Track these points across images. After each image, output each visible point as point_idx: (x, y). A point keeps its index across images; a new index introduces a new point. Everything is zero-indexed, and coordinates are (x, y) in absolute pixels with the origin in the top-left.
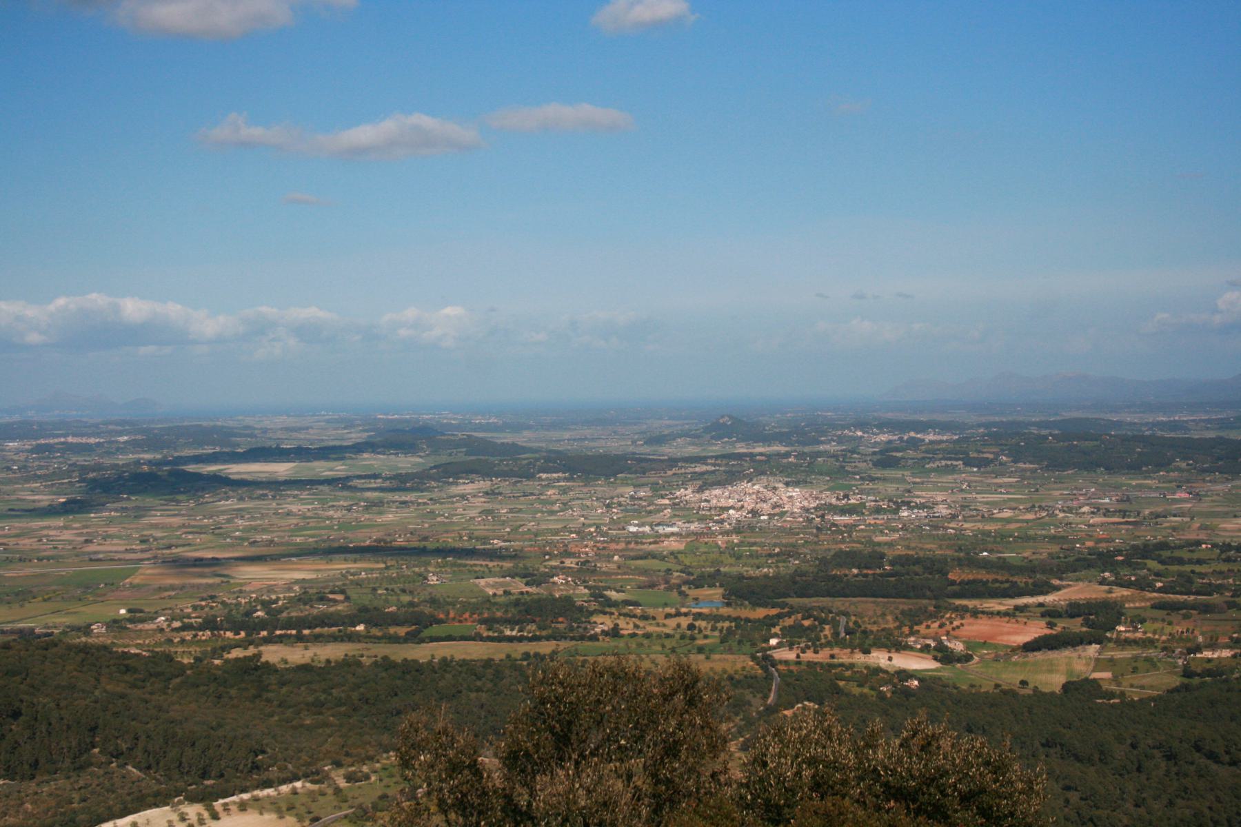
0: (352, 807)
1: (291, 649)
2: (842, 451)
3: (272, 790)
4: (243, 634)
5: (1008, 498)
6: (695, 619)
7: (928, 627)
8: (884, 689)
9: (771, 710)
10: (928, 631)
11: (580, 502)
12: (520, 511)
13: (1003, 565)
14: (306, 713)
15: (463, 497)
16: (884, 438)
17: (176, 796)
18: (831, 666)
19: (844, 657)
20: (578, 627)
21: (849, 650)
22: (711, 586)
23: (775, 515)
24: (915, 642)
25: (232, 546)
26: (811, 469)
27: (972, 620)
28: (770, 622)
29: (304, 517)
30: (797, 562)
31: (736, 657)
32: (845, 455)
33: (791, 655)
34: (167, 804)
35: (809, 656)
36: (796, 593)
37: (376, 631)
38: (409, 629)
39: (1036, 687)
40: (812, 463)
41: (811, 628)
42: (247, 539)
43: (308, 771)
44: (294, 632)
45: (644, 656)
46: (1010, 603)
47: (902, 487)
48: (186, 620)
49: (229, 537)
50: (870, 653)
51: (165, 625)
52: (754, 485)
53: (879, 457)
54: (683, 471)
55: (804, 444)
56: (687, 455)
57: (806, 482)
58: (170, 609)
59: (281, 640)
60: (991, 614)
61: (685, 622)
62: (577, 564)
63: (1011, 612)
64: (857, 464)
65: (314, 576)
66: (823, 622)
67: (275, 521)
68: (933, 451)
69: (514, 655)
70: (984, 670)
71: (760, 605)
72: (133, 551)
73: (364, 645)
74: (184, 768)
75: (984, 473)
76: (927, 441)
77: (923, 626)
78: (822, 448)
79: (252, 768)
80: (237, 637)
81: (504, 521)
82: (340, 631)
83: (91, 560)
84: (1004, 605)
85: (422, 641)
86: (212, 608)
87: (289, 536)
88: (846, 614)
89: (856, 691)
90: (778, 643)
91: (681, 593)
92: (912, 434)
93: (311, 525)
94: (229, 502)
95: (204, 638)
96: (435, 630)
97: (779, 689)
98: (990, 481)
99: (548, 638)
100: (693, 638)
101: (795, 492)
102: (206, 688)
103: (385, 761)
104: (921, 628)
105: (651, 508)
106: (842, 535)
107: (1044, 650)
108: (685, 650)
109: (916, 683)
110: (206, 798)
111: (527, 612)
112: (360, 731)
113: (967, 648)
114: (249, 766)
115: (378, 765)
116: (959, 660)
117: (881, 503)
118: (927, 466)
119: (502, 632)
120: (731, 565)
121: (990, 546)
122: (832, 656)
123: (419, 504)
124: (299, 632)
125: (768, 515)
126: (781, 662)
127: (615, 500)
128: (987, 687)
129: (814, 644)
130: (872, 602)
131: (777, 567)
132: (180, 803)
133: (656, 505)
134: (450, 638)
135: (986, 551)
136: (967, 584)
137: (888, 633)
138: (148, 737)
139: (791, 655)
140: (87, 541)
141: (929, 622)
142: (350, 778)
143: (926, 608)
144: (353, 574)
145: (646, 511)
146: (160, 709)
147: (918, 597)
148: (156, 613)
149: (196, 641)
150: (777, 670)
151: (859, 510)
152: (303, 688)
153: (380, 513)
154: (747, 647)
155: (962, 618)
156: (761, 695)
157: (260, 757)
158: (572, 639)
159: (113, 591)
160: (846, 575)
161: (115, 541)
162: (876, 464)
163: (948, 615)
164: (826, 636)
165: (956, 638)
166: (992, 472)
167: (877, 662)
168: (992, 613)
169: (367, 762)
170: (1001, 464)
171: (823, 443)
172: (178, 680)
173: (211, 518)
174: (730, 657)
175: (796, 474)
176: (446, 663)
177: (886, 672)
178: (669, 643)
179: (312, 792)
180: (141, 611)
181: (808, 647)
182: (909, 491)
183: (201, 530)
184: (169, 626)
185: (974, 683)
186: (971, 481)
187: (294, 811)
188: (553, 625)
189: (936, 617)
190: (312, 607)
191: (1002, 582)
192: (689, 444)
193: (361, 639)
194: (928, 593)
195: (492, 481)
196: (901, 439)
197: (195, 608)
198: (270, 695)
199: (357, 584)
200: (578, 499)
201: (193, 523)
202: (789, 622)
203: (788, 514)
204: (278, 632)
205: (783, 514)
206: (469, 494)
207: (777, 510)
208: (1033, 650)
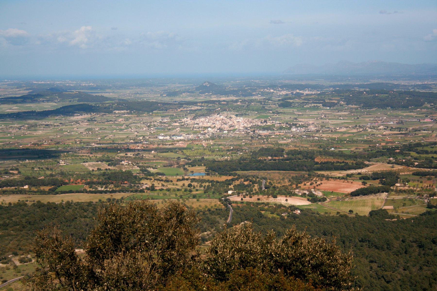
0: (23, 275)
2: (263, 99)
5: (344, 122)
6: (191, 182)
7: (305, 185)
9: (229, 226)
10: (305, 187)
11: (135, 124)
13: (341, 155)
15: (77, 122)
16: (284, 93)
18: (258, 204)
19: (264, 199)
20: (134, 186)
21: (267, 196)
23: (230, 130)
26: (248, 108)
27: (326, 181)
28: (228, 183)
30: (241, 153)
31: (212, 200)
35: (247, 199)
36: (241, 169)
37: (34, 189)
39: (357, 213)
41: (248, 186)
47: (293, 117)
50: (277, 198)
52: (220, 116)
53: (281, 102)
54: (186, 109)
55: (245, 96)
60: (335, 178)
61: (187, 183)
63: (345, 177)
66: (254, 182)
68: (308, 99)
71: (224, 175)
75: (332, 110)
76: (305, 94)
81: (97, 134)
84: (342, 174)
85: (57, 193)
88: (265, 179)
89: (270, 216)
90: (232, 193)
91: (185, 169)
92: (298, 91)
98: (335, 114)
99: (119, 191)
100: (191, 191)
101: (241, 119)
104: (302, 185)
105: (170, 127)
106: (263, 140)
107: (361, 195)
109: (299, 212)
113: (324, 195)
117: (282, 125)
118: (305, 107)
119: (97, 189)
120: (209, 155)
121: (335, 145)
123: (55, 126)
125: (228, 130)
126: (233, 202)
127: (152, 124)
128: (333, 213)
130: (278, 173)
131: (232, 156)
133: (173, 126)
134: (71, 192)
135: (333, 147)
136: (324, 164)
137: (285, 187)
141: (306, 183)
142: (21, 261)
145: (168, 129)
147: (300, 170)
150: (232, 206)
151: (272, 128)
153: (35, 130)
154: (217, 195)
155: (322, 180)
156: (224, 218)
158: (132, 191)
160: (265, 160)
163: (314, 179)
164: (255, 190)
165: (318, 190)
167: (280, 201)
168: (336, 178)
169: (30, 253)
170: (341, 105)
171: (254, 95)
174: (209, 200)
176: (69, 204)
177: (285, 207)
178: (179, 194)
181: (247, 195)
182: (296, 119)
185: (327, 212)
186: (326, 114)
188: (122, 185)
191: (341, 163)
192: (189, 96)
193: (27, 192)
194: (305, 168)
195: (91, 114)
196: (292, 93)
199: (24, 166)
200: (134, 123)
202: (237, 183)
203: (237, 130)
207: (232, 128)
208: (356, 196)
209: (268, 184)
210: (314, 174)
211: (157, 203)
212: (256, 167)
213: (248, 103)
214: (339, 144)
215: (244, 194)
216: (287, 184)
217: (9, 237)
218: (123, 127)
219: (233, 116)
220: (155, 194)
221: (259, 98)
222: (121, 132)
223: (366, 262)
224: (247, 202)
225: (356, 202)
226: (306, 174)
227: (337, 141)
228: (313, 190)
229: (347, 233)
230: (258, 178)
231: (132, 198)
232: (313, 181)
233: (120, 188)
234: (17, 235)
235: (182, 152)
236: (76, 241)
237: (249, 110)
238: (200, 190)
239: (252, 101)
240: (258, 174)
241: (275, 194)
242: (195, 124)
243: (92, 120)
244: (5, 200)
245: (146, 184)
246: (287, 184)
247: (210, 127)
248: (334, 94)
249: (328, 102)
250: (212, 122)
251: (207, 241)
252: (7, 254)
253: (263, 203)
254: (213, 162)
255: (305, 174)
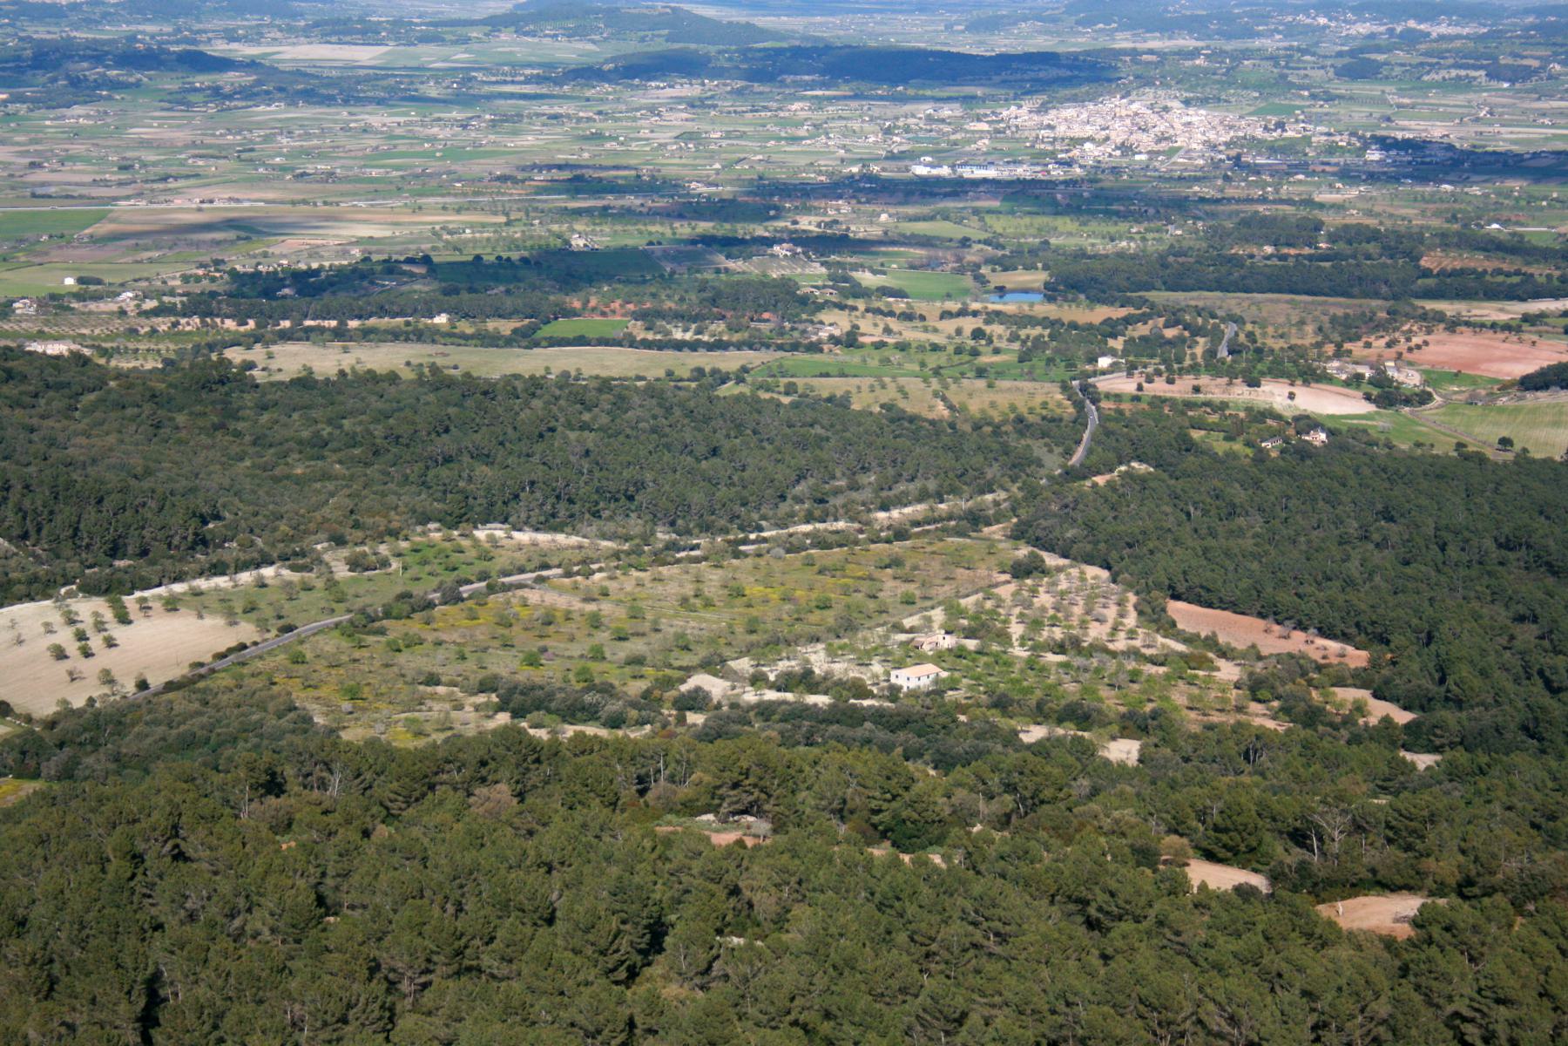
0: (349, 611)
1: (322, 350)
2: (1286, 49)
3: (226, 578)
4: (252, 324)
5: (1555, 135)
6: (987, 322)
7: (1368, 345)
8: (1267, 445)
9: (1071, 475)
10: (1367, 352)
11: (843, 123)
12: (743, 136)
13: (1516, 248)
14: (297, 456)
15: (653, 110)
16: (1363, 29)
17: (64, 585)
18: (1189, 405)
19: (1214, 389)
20: (793, 329)
21: (1226, 380)
22: (1029, 267)
23: (1158, 153)
24: (1340, 370)
25: (265, 179)
26: (1230, 79)
27: (1444, 336)
28: (1111, 329)
29: (391, 137)
30: (1179, 232)
31: (1037, 385)
32: (1291, 56)
33: (1126, 385)
34: (47, 597)
35: (1159, 387)
36: (1165, 283)
37: (466, 327)
38: (518, 325)
39: (1525, 450)
40: (1233, 68)
41: (1178, 342)
42: (293, 169)
43: (289, 551)
44: (334, 323)
45: (887, 380)
46: (1516, 309)
47: (1377, 112)
48: (166, 299)
49: (264, 164)
50: (1259, 386)
51: (130, 307)
52: (1132, 102)
53: (1347, 60)
54: (1019, 76)
55: (1229, 36)
56: (873, 44)
57: (1219, 100)
58: (147, 279)
59: (307, 335)
60: (1479, 326)
61: (969, 324)
62: (819, 225)
63: (1514, 323)
64: (1308, 72)
65: (388, 233)
66: (1196, 331)
67: (342, 140)
68: (1439, 54)
69: (678, 373)
70: (1446, 419)
71: (1103, 302)
72: (106, 184)
73: (440, 348)
74: (82, 539)
75: (1519, 91)
76: (1434, 35)
77: (1361, 344)
78: (1257, 43)
79: (195, 543)
80: (242, 329)
81: (713, 151)
82: (408, 324)
83: (34, 195)
84: (1508, 312)
85: (537, 344)
86: (213, 280)
87: (361, 167)
88: (1239, 320)
89: (1220, 446)
90: (1112, 365)
91: (979, 278)
92: (1412, 24)
93: (402, 149)
94: (273, 108)
95: (188, 328)
96: (561, 327)
97: (1093, 438)
98: (1527, 105)
99: (739, 346)
100: (975, 353)
101: (1198, 116)
102: (136, 410)
103: (418, 539)
104: (1356, 348)
105: (958, 136)
106: (1263, 189)
107: (1553, 388)
108: (955, 372)
109: (1323, 436)
110: (109, 588)
111: (714, 301)
112: (381, 488)
113: (1426, 382)
114: (190, 538)
115: (404, 545)
116: (1407, 401)
117: (1337, 138)
118: (1426, 78)
119: (669, 333)
120: (1070, 234)
121: (1506, 214)
122: (1197, 389)
123: (579, 120)
124: (342, 323)
125: (1149, 152)
126: (1108, 396)
127: (900, 123)
128: (1444, 448)
129: (1169, 368)
130: (1287, 302)
131: (1144, 239)
132: (70, 595)
133: (967, 132)
134: (581, 341)
135: (1497, 221)
136: (1450, 275)
137: (1298, 352)
138: (27, 487)
139: (1126, 385)
140: (33, 165)
141: (1372, 339)
142: (355, 564)
143: (1374, 314)
144: (450, 233)
145: (948, 142)
146: (52, 443)
147: (1366, 295)
148: (122, 285)
149: (174, 334)
150: (1098, 409)
151: (1299, 148)
152: (295, 416)
153: (515, 133)
154: (1059, 371)
155: (1429, 332)
156: (1060, 450)
157: (211, 526)
158: (780, 347)
159: (61, 247)
160: (1252, 256)
161: (79, 166)
162: (1342, 73)
163: (1406, 328)
164: (1193, 356)
165: (1410, 364)
166: (1534, 90)
167: (1270, 400)
168: (1482, 325)
169: (387, 538)
170: (1550, 77)
171: (1259, 35)
172: (92, 397)
173: (239, 133)
174: (1027, 385)
175: (1204, 86)
176: (535, 385)
177: (1278, 417)
178: (933, 360)
179: (288, 585)
180: (99, 282)
181: (1158, 373)
182: (1389, 119)
183: (220, 153)
184: (138, 306)
185: (1421, 440)
186: (1496, 105)
187: (253, 615)
188: (753, 325)
189: (1386, 330)
190: (372, 283)
191: (1508, 275)
192: (1039, 32)
193: (437, 337)
194: (1384, 289)
195: (703, 84)
196: (1391, 31)
197: (186, 279)
198: (241, 426)
199: (456, 249)
200: (841, 118)
201: (208, 140)
202: (1142, 330)
203: (1181, 153)
204: (308, 323)
205: (1173, 151)
206: (661, 105)
207: (1164, 146)
208: (1537, 388)
209: (1242, 338)
210: (1408, 309)
211: (854, 390)
212: (1218, 281)
213: (1233, 59)
214: (1522, 209)
215: (1150, 370)
216: (1309, 337)
217: (327, 484)
218: (802, 132)
219: (1175, 104)
220: (853, 358)
221: (1273, 44)
222: (794, 148)
223: (1503, 615)
224: (1155, 397)
225: (1533, 411)
226: (1381, 309)
227: (1517, 199)
228: (1391, 364)
229: (1461, 518)
230: (1213, 316)
231: (775, 370)
232: (1397, 335)
233: (746, 335)
234: (352, 478)
235: (982, 220)
236: (542, 505)
237: (1230, 85)
238: (1008, 351)
239: (1246, 54)
240: (1218, 303)
241: (1255, 374)
242: (1042, 127)
243: (703, 106)
244: (363, 358)
245: (834, 323)
246: (1309, 337)
247: (1090, 139)
248: (1532, 37)
249: (1506, 66)
250: (1100, 121)
251: (989, 524)
252: (313, 537)
253: (1207, 404)
254: (1076, 257)
255: (1378, 307)
